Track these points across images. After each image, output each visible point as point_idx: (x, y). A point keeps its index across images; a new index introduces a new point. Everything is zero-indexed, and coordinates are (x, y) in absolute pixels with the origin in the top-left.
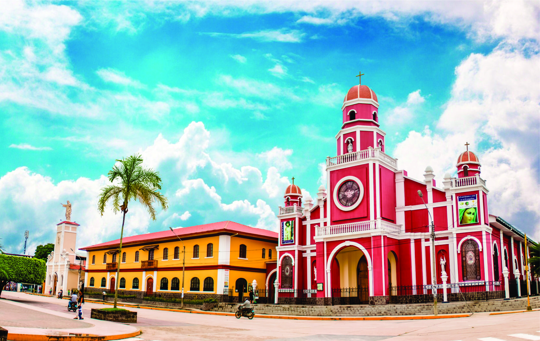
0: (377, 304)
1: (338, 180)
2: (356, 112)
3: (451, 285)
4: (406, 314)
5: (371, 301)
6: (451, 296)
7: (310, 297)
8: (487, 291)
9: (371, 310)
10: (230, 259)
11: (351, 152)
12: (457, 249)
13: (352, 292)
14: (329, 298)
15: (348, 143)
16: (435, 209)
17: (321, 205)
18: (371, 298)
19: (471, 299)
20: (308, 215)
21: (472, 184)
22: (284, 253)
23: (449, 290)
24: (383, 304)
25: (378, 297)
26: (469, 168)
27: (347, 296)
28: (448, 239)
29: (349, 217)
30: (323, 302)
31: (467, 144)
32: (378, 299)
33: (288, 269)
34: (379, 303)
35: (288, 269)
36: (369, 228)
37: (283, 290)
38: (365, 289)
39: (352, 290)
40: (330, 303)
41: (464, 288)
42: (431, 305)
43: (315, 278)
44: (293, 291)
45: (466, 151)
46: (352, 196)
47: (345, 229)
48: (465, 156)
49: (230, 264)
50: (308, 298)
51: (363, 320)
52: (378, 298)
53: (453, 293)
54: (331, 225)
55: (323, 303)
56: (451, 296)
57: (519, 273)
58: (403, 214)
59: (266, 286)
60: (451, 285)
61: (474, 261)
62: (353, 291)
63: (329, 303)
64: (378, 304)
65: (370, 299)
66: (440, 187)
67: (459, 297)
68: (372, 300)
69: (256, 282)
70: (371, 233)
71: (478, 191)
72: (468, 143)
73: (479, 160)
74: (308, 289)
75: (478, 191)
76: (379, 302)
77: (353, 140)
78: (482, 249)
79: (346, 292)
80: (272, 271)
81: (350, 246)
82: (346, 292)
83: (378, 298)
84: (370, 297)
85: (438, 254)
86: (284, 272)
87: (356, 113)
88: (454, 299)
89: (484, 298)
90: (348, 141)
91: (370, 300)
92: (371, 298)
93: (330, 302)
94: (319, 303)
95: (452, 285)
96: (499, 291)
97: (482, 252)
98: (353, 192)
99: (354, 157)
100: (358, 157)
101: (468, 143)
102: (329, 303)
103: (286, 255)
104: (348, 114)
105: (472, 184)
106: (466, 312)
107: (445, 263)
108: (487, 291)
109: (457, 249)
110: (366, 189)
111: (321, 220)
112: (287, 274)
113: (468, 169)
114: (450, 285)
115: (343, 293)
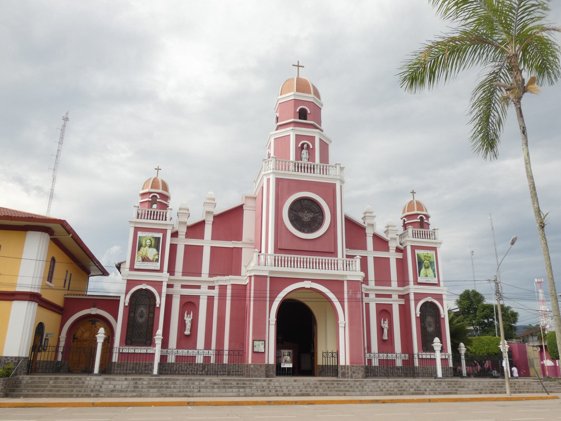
0: (355, 376)
1: (290, 194)
2: (309, 112)
3: (239, 353)
4: (284, 394)
5: (343, 372)
6: (396, 370)
7: (173, 362)
8: (224, 363)
9: (383, 386)
10: (162, 286)
11: (305, 161)
12: (125, 299)
13: (331, 358)
14: (320, 365)
15: (302, 147)
16: (213, 249)
17: (209, 221)
18: (343, 367)
19: (230, 373)
20: (183, 231)
21: (162, 220)
22: (141, 284)
23: (163, 358)
24: (360, 377)
25: (357, 366)
26: (159, 199)
27: (376, 365)
28: (200, 289)
29: (306, 247)
30: (263, 372)
31: (158, 169)
32: (357, 370)
33: (144, 311)
34: (359, 376)
35: (144, 311)
36: (337, 267)
37: (127, 350)
38: (332, 354)
39: (330, 354)
40: (273, 373)
41: (127, 354)
42: (385, 381)
43: (185, 330)
44: (381, 355)
45: (156, 176)
46: (310, 219)
47: (305, 264)
48: (155, 184)
49: (41, 292)
50: (197, 364)
51: (428, 402)
52: (358, 368)
53: (399, 366)
54: (275, 252)
55: (264, 373)
56: (396, 370)
57: (440, 344)
58: (183, 247)
59: (61, 340)
60: (239, 353)
61: (434, 328)
62: (332, 355)
63: (271, 373)
64: (356, 377)
65: (342, 369)
66: (380, 230)
67: (420, 372)
68: (343, 370)
69: (104, 332)
70: (348, 276)
71: (167, 230)
72: (157, 168)
73: (428, 210)
74: (170, 347)
75: (167, 230)
76: (358, 374)
77: (311, 147)
78: (160, 305)
79: (237, 356)
80: (86, 310)
81: (311, 289)
82: (237, 356)
83: (358, 368)
84: (341, 366)
85: (183, 306)
86: (134, 317)
87: (309, 114)
88: (401, 374)
89: (448, 375)
90: (303, 145)
91: (341, 370)
92: (343, 367)
93: (273, 372)
94: (256, 374)
95: (398, 355)
96: (383, 366)
97: (159, 308)
98: (311, 215)
99: (312, 169)
100: (317, 171)
101: (159, 168)
102: (271, 373)
103: (144, 288)
104: (298, 110)
105: (162, 220)
106: (517, 392)
107: (192, 320)
108: (224, 363)
109: (125, 299)
110: (333, 217)
111: (182, 242)
112: (141, 320)
113: (158, 200)
114: (394, 355)
115: (326, 358)
